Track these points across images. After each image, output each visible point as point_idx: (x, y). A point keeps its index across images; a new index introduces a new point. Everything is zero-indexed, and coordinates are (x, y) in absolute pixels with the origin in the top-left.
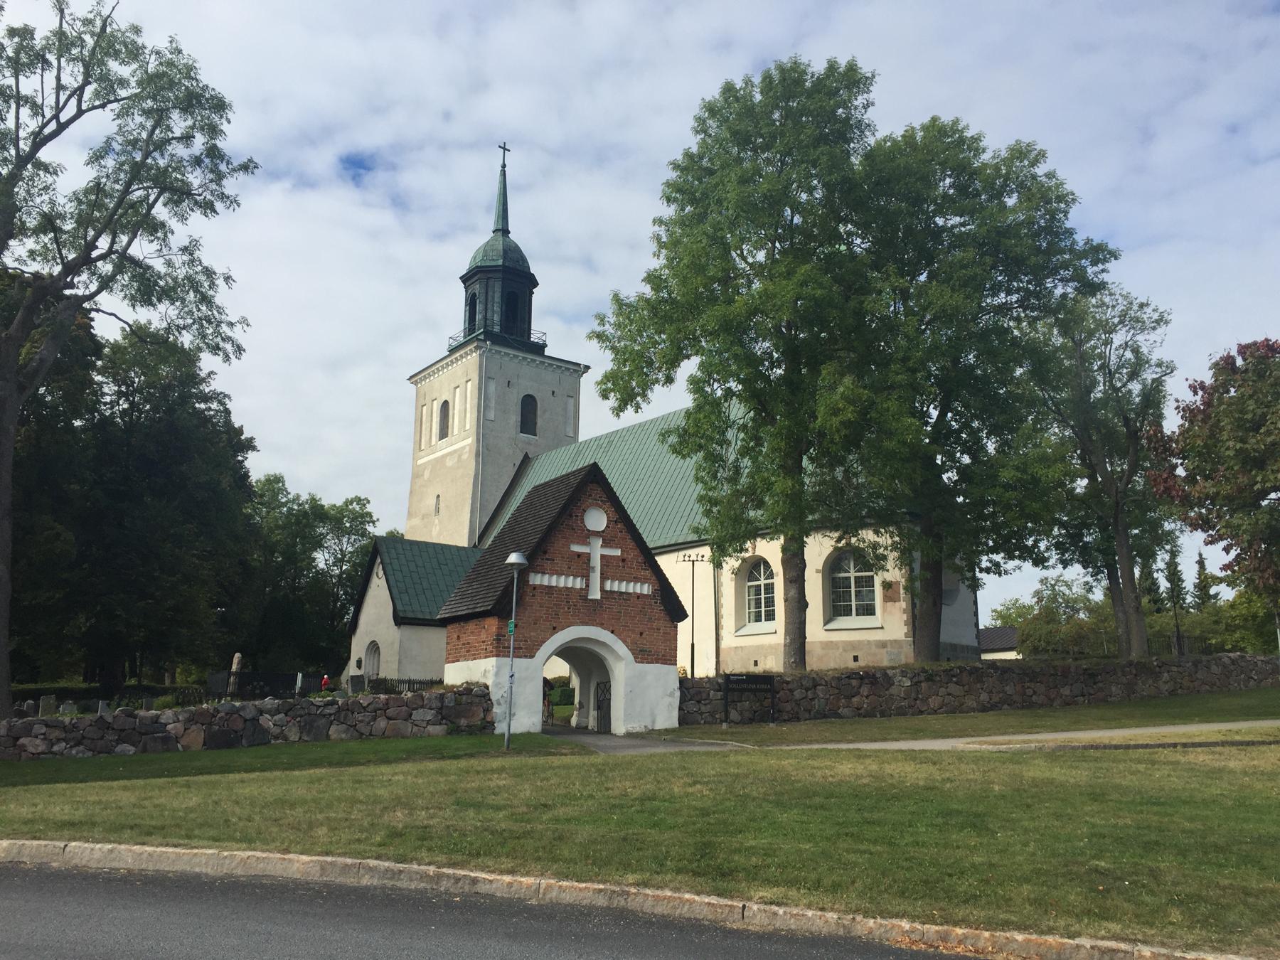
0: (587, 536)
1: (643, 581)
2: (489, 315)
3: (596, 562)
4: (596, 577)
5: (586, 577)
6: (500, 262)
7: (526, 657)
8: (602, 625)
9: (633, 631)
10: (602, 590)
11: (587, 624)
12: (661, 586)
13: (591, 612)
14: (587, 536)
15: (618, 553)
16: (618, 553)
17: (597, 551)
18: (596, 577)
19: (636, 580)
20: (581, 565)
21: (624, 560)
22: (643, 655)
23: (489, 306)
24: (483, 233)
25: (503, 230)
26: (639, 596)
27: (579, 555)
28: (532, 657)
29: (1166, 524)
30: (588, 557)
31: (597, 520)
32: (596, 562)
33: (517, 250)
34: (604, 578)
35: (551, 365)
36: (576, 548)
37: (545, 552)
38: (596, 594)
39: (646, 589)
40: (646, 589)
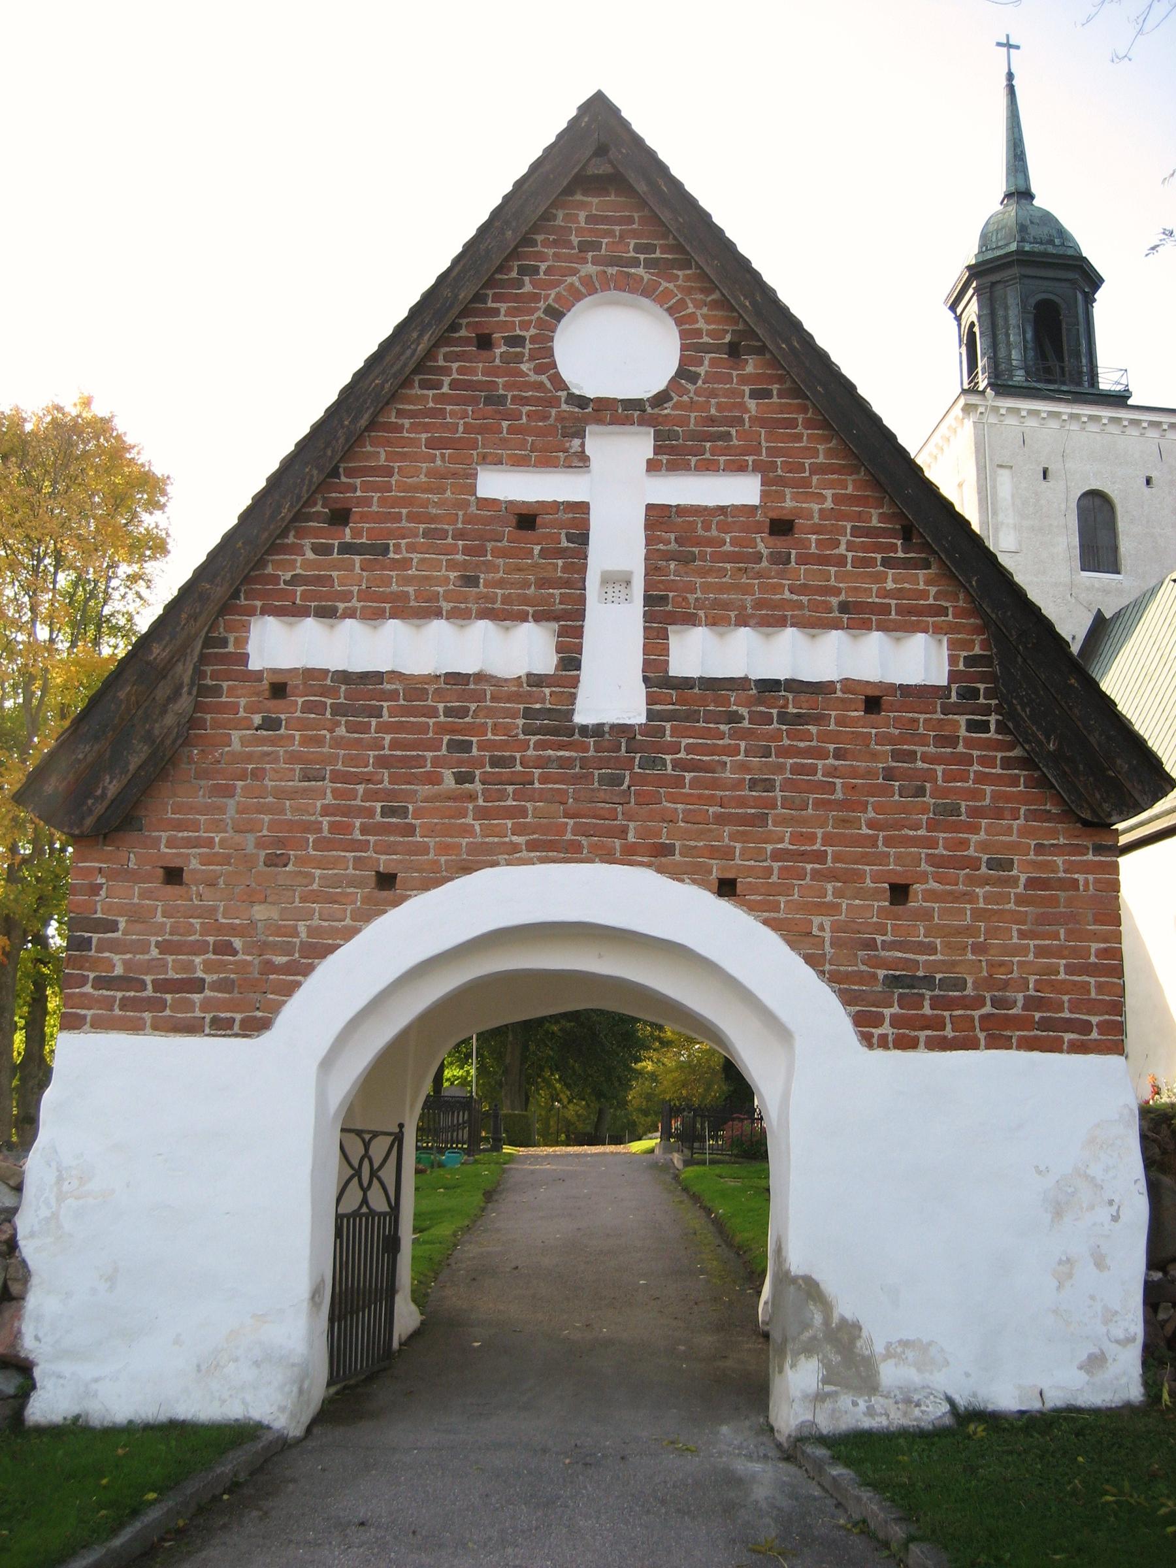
0: (565, 424)
1: (901, 619)
2: (1002, 353)
3: (617, 546)
4: (614, 632)
5: (569, 624)
6: (1013, 247)
7: (221, 1027)
8: (658, 855)
9: (849, 878)
10: (656, 677)
11: (570, 852)
12: (992, 629)
13: (599, 790)
14: (565, 424)
15: (741, 490)
16: (741, 490)
17: (617, 490)
18: (614, 632)
19: (857, 616)
20: (541, 561)
21: (781, 527)
22: (905, 1005)
23: (1001, 337)
24: (987, 199)
25: (1020, 193)
26: (874, 700)
27: (526, 518)
28: (256, 1026)
29: (761, 1492)
30: (575, 520)
31: (617, 346)
32: (617, 546)
33: (1047, 219)
34: (663, 614)
35: (1135, 423)
36: (502, 485)
37: (340, 517)
38: (612, 695)
39: (917, 660)
40: (917, 660)
